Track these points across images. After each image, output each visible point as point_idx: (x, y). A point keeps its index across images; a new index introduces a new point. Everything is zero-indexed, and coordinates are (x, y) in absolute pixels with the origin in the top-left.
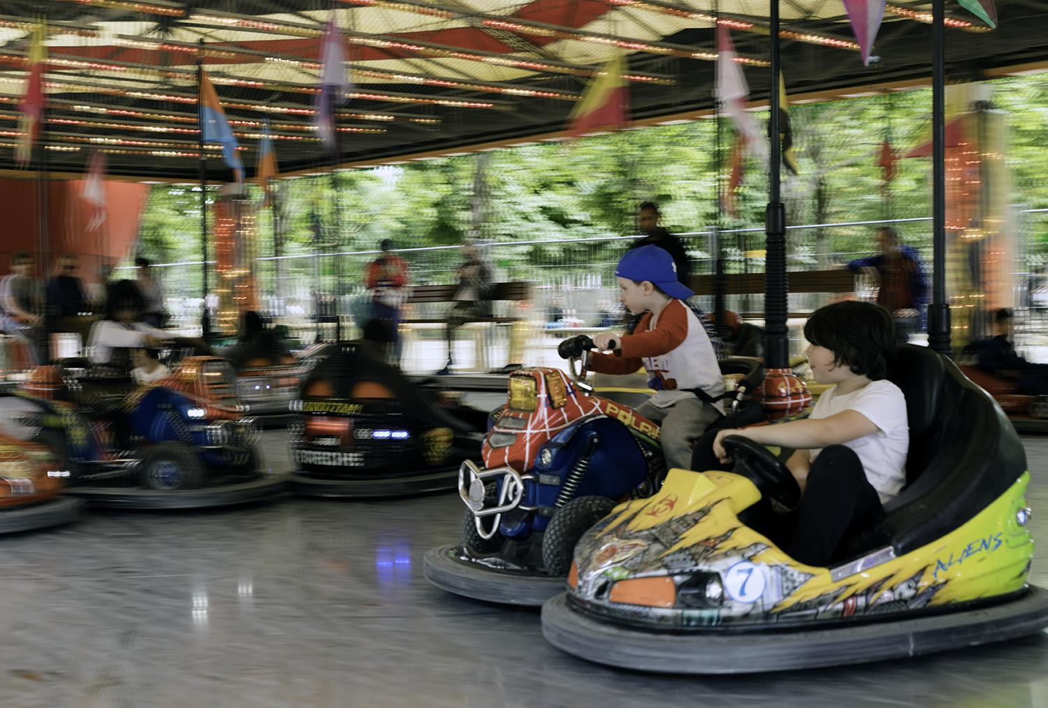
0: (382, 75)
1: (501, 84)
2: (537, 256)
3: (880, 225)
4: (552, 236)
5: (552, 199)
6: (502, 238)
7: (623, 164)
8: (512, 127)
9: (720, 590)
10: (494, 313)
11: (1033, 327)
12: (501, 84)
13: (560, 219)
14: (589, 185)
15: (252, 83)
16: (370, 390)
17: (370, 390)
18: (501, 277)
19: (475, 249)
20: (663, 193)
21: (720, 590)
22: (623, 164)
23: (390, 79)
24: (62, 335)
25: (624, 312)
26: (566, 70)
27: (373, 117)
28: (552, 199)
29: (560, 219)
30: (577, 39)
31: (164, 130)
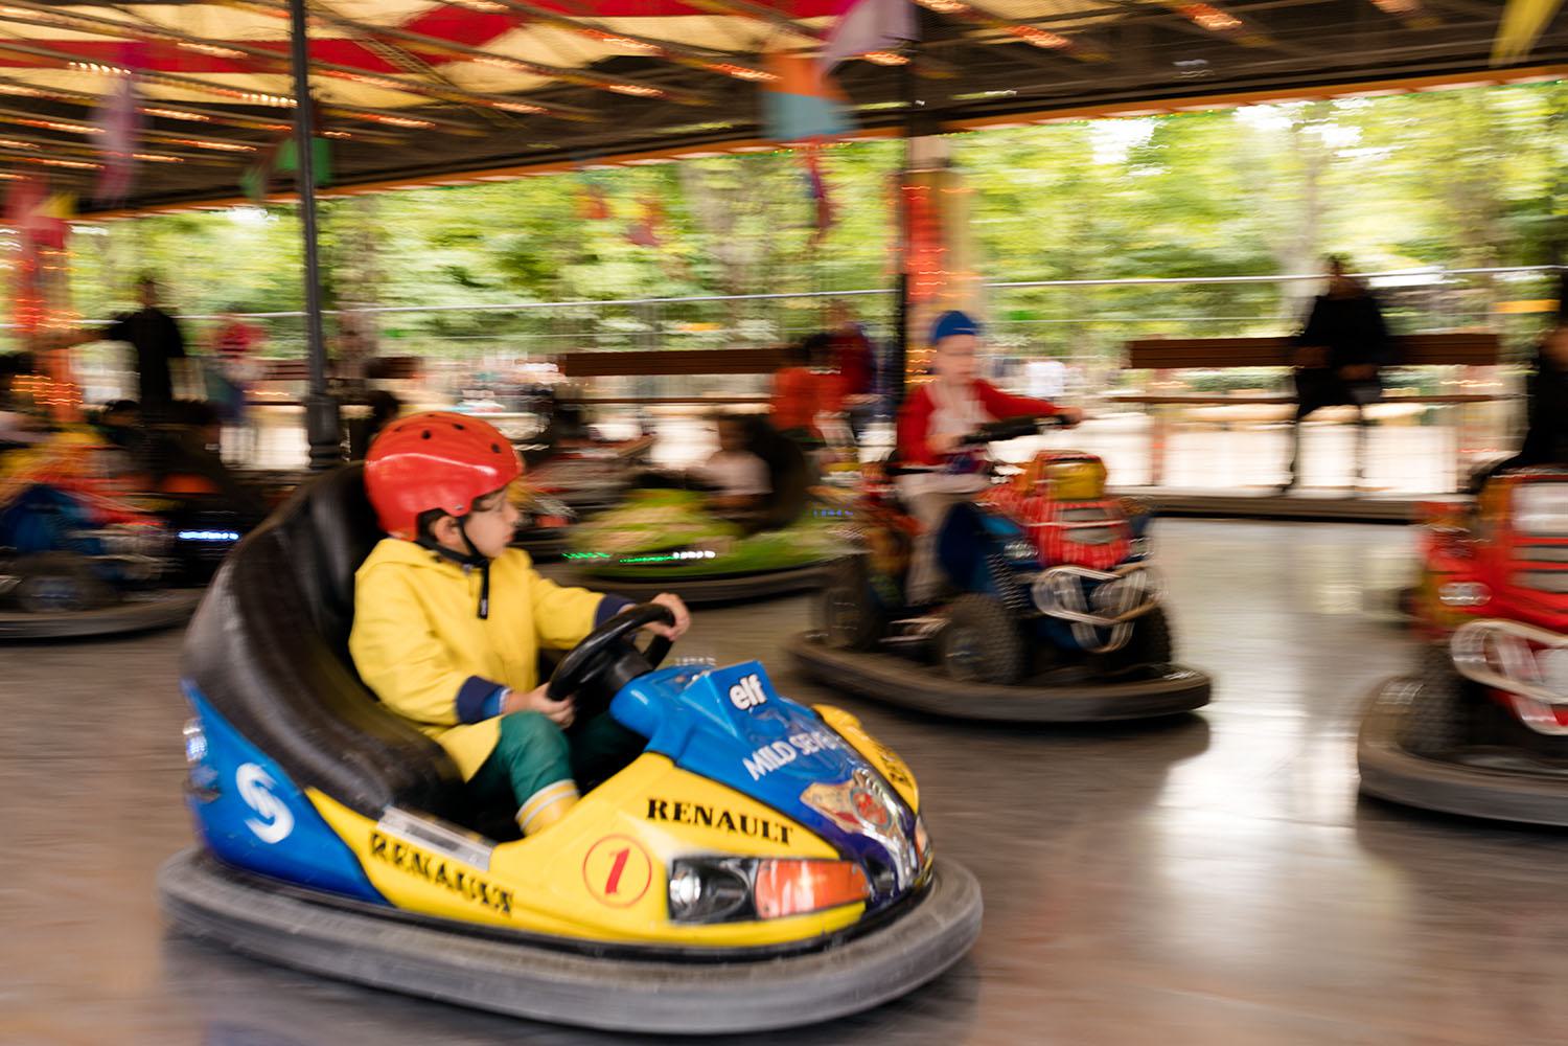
0: (230, 92)
1: (383, 112)
2: (441, 328)
3: (83, 327)
4: (459, 303)
5: (461, 257)
6: (391, 303)
7: (1418, 185)
8: (395, 165)
9: (674, 884)
10: (863, 429)
11: (593, 468)
12: (383, 112)
13: (463, 279)
14: (506, 239)
15: (67, 96)
16: (187, 486)
17: (187, 486)
18: (388, 349)
19: (350, 315)
20: (587, 253)
21: (674, 884)
22: (1418, 185)
23: (239, 97)
24: (894, 433)
25: (860, 437)
26: (463, 99)
27: (209, 145)
28: (461, 257)
29: (463, 279)
30: (468, 60)
31: (186, 116)
